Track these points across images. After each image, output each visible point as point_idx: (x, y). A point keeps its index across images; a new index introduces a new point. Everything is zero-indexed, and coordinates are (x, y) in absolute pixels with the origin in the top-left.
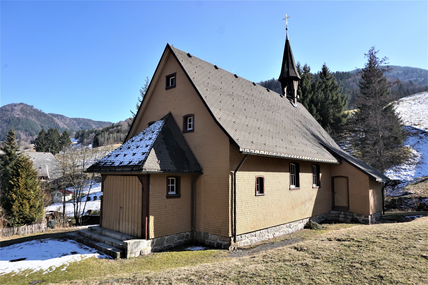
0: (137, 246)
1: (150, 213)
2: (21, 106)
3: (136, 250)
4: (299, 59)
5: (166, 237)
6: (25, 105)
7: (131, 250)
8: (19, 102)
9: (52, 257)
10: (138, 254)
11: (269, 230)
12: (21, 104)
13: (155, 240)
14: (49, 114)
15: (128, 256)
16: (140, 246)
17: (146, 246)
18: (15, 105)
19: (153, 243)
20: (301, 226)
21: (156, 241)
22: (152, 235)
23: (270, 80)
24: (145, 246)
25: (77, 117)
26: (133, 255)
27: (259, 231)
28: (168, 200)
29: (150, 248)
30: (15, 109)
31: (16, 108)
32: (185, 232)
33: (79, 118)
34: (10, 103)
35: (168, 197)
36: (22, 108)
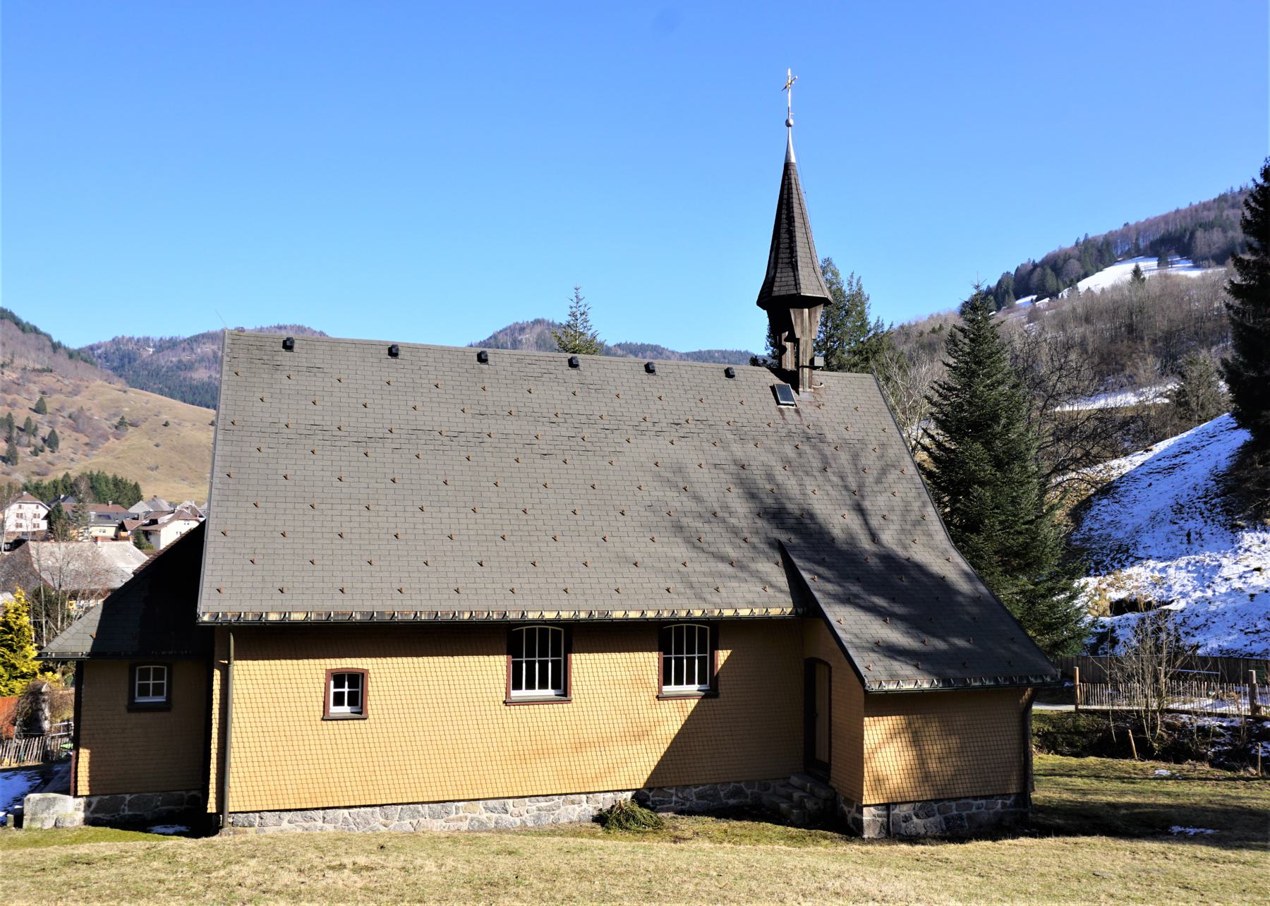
0: (48, 808)
1: (82, 742)
2: (538, 329)
3: (45, 815)
4: (838, 248)
5: (128, 797)
6: (548, 324)
7: (34, 814)
8: (531, 319)
9: (208, 789)
10: (49, 824)
11: (388, 809)
12: (537, 322)
13: (95, 800)
14: (619, 345)
15: (25, 824)
16: (57, 808)
17: (70, 810)
18: (522, 329)
19: (88, 805)
20: (588, 808)
21: (99, 802)
22: (83, 788)
23: (1143, 220)
24: (71, 809)
25: (704, 349)
26: (37, 825)
27: (346, 811)
28: (133, 715)
29: (81, 815)
30: (520, 341)
31: (523, 337)
32: (187, 791)
33: (709, 352)
34: (509, 323)
35: (133, 708)
36: (539, 336)
